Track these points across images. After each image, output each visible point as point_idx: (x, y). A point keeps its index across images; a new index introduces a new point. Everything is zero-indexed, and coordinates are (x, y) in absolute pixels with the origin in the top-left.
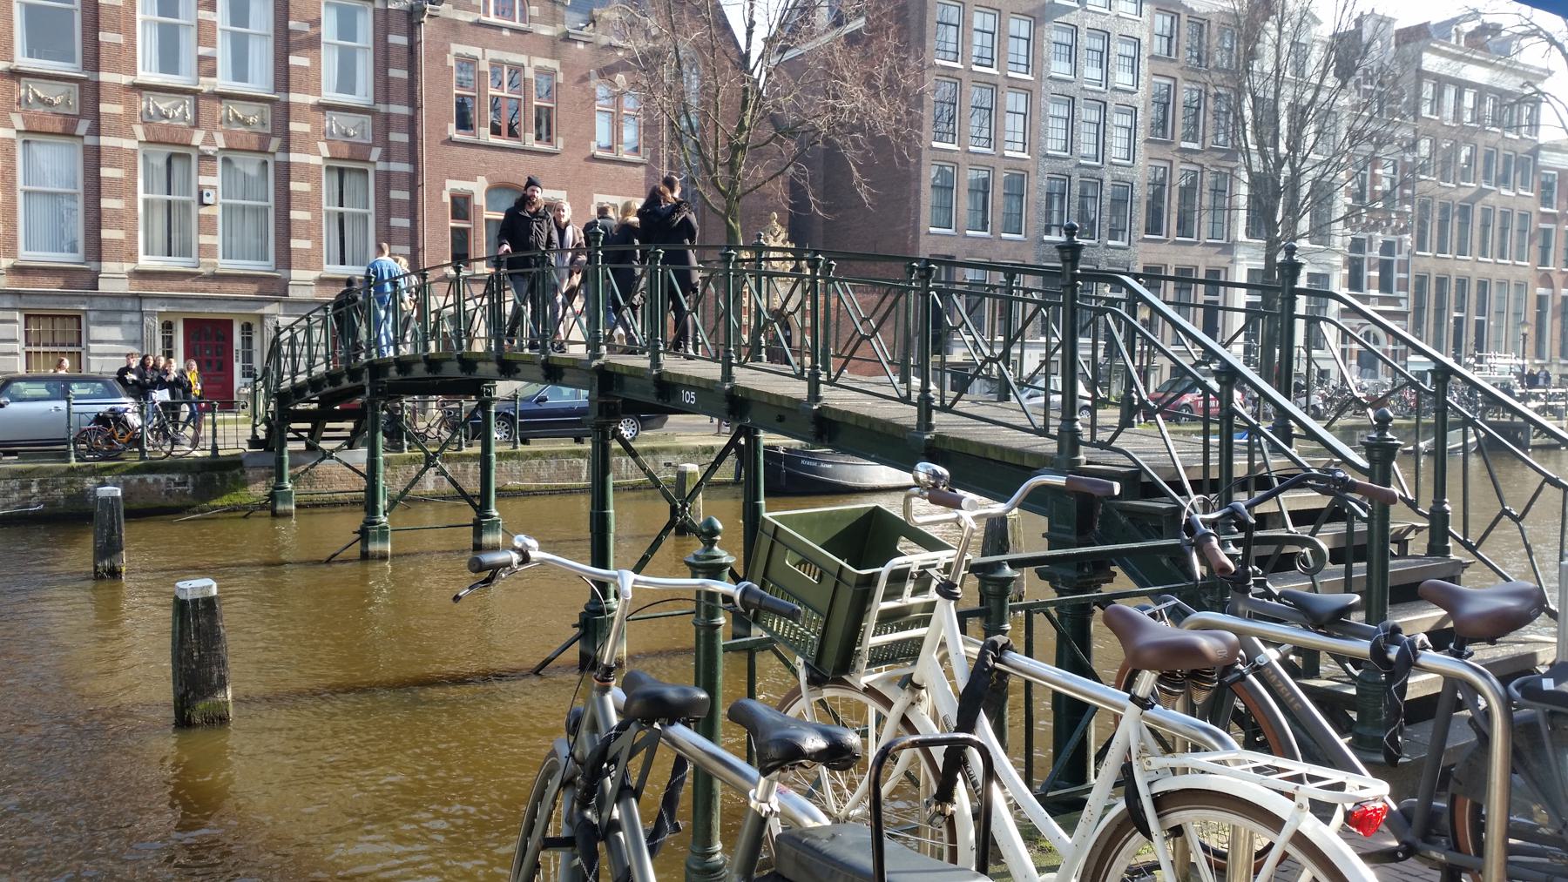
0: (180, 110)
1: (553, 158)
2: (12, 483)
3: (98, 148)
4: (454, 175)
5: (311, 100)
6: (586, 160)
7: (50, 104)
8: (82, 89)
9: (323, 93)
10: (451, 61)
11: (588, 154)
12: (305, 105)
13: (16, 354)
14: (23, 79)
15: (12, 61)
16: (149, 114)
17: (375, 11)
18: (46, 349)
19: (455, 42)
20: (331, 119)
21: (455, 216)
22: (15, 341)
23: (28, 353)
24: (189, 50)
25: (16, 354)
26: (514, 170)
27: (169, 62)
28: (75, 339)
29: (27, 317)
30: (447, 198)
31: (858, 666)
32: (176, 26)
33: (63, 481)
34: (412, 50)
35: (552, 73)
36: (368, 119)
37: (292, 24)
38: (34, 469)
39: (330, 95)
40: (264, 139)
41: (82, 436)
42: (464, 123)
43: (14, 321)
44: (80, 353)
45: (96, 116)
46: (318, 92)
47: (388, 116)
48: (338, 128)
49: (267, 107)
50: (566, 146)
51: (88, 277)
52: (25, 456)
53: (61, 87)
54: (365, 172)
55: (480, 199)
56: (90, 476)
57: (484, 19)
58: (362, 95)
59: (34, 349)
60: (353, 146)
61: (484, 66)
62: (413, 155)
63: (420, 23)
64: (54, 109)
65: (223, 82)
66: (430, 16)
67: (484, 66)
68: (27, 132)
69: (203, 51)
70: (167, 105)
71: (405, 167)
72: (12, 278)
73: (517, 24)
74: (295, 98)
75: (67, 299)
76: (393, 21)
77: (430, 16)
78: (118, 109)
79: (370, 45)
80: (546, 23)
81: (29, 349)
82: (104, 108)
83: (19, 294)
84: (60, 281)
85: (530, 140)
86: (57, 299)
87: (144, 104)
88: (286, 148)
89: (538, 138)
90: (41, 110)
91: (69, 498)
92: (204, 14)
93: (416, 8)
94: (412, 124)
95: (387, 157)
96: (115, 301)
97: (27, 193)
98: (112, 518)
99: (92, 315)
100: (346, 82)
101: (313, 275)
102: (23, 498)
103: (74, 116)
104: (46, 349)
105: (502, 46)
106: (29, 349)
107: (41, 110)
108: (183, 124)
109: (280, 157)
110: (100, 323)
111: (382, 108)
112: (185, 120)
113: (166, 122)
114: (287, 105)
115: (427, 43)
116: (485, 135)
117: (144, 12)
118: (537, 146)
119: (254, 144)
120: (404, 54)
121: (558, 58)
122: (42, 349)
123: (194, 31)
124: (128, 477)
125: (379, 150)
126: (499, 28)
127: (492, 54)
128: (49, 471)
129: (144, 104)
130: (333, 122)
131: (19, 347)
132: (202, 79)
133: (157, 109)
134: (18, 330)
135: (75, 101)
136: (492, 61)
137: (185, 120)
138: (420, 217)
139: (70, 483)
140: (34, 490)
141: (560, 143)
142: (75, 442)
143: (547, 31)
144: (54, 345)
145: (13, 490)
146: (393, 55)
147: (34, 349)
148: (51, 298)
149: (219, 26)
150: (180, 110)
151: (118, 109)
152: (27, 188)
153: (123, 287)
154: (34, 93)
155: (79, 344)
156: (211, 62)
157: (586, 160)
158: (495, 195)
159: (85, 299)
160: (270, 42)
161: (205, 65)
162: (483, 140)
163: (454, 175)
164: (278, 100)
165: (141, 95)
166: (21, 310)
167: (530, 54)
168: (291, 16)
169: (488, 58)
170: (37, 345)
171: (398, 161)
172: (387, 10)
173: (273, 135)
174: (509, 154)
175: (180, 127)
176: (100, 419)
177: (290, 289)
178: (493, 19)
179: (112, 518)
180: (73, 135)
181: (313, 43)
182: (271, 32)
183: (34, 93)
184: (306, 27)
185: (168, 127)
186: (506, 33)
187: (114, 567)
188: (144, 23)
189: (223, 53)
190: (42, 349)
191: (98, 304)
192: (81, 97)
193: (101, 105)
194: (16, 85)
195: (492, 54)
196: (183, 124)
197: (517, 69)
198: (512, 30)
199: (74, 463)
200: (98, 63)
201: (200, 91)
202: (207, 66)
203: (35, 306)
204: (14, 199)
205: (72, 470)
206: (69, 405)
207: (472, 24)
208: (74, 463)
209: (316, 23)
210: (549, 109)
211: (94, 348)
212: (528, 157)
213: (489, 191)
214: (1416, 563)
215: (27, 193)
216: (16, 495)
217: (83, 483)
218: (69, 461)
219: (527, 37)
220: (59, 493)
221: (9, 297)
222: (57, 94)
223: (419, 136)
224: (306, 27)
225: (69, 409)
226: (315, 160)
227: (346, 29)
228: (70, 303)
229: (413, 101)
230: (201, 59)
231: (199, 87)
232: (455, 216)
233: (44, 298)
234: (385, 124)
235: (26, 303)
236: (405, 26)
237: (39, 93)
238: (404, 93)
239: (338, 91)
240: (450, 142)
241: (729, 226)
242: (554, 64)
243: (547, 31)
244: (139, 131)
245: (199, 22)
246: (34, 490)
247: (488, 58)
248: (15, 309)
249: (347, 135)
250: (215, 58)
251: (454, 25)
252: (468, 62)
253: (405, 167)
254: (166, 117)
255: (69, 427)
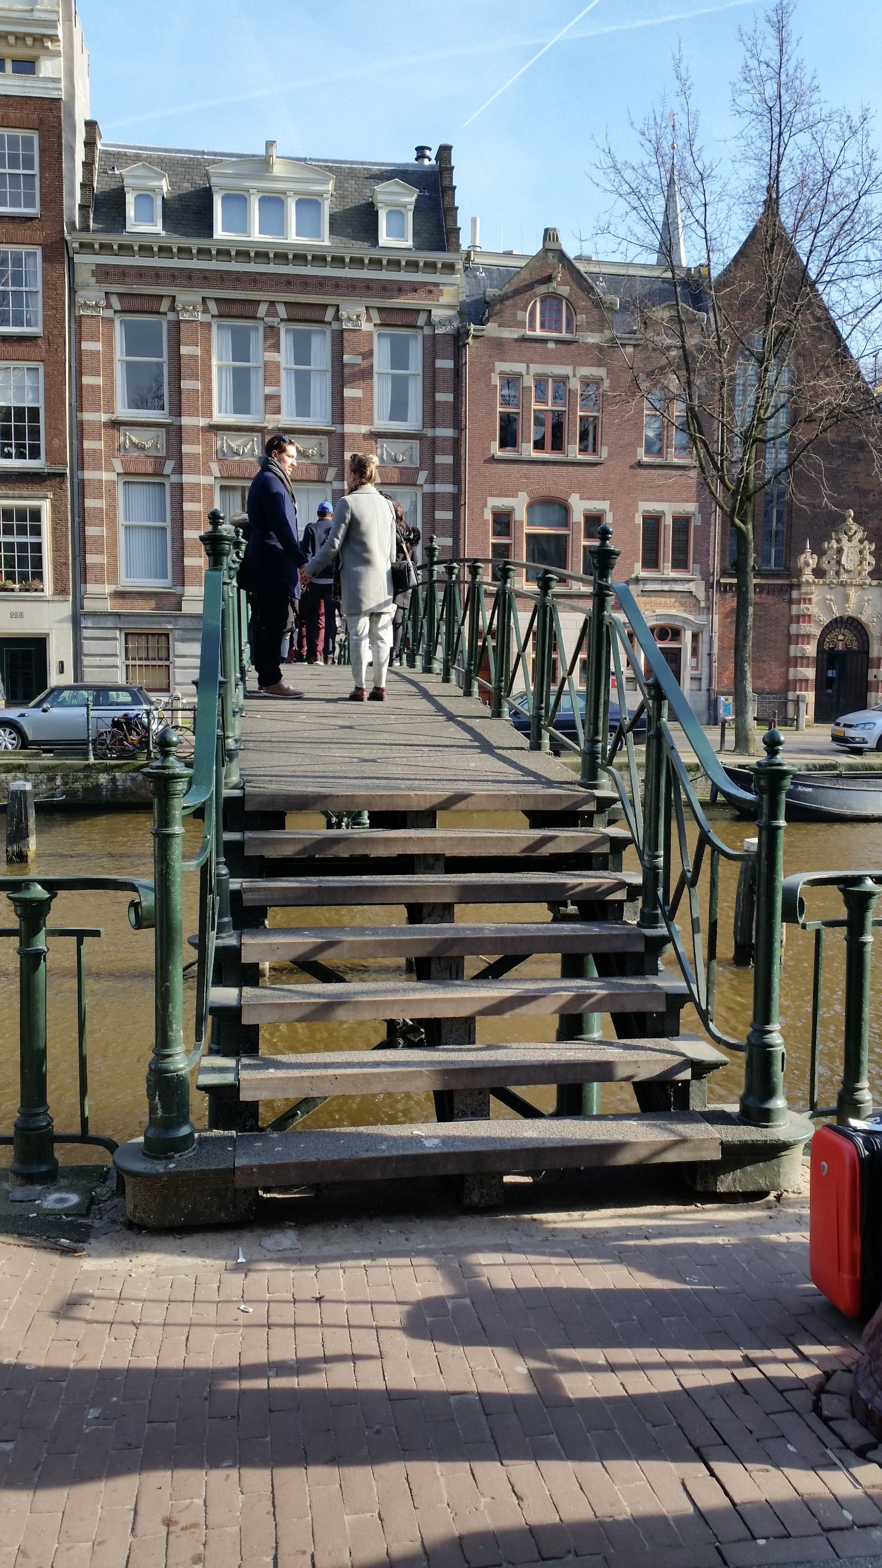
0: (249, 447)
1: (597, 468)
2: (41, 776)
3: (180, 486)
4: (496, 492)
5: (364, 429)
6: (632, 467)
7: (143, 448)
8: (168, 433)
9: (376, 421)
10: (496, 380)
11: (634, 462)
12: (358, 434)
13: (117, 667)
14: (122, 428)
15: (113, 413)
16: (223, 451)
17: (424, 337)
18: (141, 663)
19: (501, 360)
20: (382, 447)
21: (496, 533)
22: (116, 655)
23: (127, 666)
24: (259, 390)
25: (117, 667)
26: (556, 483)
27: (241, 404)
28: (163, 654)
29: (127, 635)
30: (488, 516)
31: (593, 1029)
32: (248, 369)
33: (81, 775)
34: (458, 373)
35: (598, 382)
36: (416, 444)
37: (347, 358)
38: (58, 765)
39: (382, 423)
40: (160, 462)
41: (98, 741)
42: (508, 438)
43: (115, 639)
44: (168, 666)
45: (179, 457)
46: (370, 421)
47: (434, 439)
48: (388, 454)
49: (324, 439)
50: (610, 455)
51: (173, 600)
52: (59, 754)
53: (152, 433)
54: (163, 484)
55: (521, 515)
56: (103, 772)
57: (529, 333)
58: (413, 422)
59: (131, 662)
60: (403, 471)
61: (529, 381)
62: (457, 479)
63: (465, 345)
64: (146, 452)
65: (287, 418)
66: (475, 337)
67: (529, 381)
68: (126, 474)
69: (269, 390)
70: (239, 442)
71: (449, 488)
72: (114, 601)
73: (564, 335)
74: (349, 428)
75: (156, 619)
76: (439, 346)
77: (475, 337)
78: (198, 449)
79: (420, 372)
80: (593, 331)
81: (127, 662)
82: (186, 449)
83: (118, 615)
84: (153, 603)
85: (573, 451)
86: (149, 619)
87: (219, 443)
88: (179, 470)
89: (583, 450)
90: (136, 454)
91: (86, 790)
92: (270, 356)
93: (462, 331)
94: (456, 445)
95: (432, 480)
96: (195, 620)
97: (127, 528)
98: (20, 809)
99: (176, 632)
100: (398, 411)
101: (108, 589)
102: (50, 790)
103: (414, 468)
104: (141, 663)
105: (547, 359)
106: (127, 662)
107: (136, 454)
108: (251, 459)
109: (174, 479)
110: (183, 640)
111: (429, 432)
112: (253, 455)
113: (237, 458)
114: (342, 435)
115: (471, 364)
116: (528, 450)
117: (220, 358)
118: (580, 457)
119: (314, 475)
120: (450, 377)
121: (605, 365)
122: (138, 663)
123: (261, 371)
124: (134, 774)
125: (173, 462)
126: (544, 341)
127: (536, 368)
128: (70, 767)
129: (219, 443)
130: (387, 447)
131: (120, 661)
132: (268, 416)
133: (229, 446)
134: (119, 646)
135: (162, 444)
136: (536, 375)
137: (253, 455)
138: (462, 536)
139: (86, 777)
140: (59, 782)
141: (604, 452)
142: (94, 742)
143: (593, 338)
144: (147, 659)
145: (42, 782)
146: (439, 377)
147: (131, 662)
148: (144, 619)
149: (283, 365)
150: (249, 447)
151: (198, 449)
152: (128, 523)
153: (108, 606)
154: (227, 443)
155: (168, 659)
156: (275, 401)
157: (632, 467)
158: (538, 510)
159: (171, 619)
160: (329, 375)
161: (272, 403)
162: (524, 456)
163: (496, 492)
164: (334, 432)
165: (216, 435)
166: (120, 629)
167: (575, 364)
168: (346, 350)
169: (532, 373)
170: (134, 659)
171: (443, 483)
172: (435, 335)
173: (330, 465)
174: (551, 467)
175: (250, 462)
176: (116, 724)
177: (183, 603)
178: (539, 333)
179: (20, 809)
180: (324, 482)
181: (365, 374)
182: (329, 368)
183: (130, 439)
184: (358, 360)
185: (239, 463)
186: (551, 345)
187: (21, 852)
188: (220, 368)
189: (286, 390)
190: (138, 663)
191: (181, 623)
192: (167, 440)
193: (183, 446)
194: (116, 434)
195: (536, 368)
196: (251, 459)
197: (562, 381)
198: (558, 341)
199: (92, 760)
200: (343, 417)
201: (265, 428)
202: (272, 403)
203: (132, 626)
204: (115, 533)
205: (88, 766)
206: (88, 711)
207: (517, 340)
208: (92, 760)
209: (368, 355)
210: (595, 418)
211: (179, 662)
212: (571, 469)
213: (530, 507)
214: (279, 997)
215: (127, 528)
216: (44, 787)
217: (97, 778)
218: (87, 759)
219: (573, 347)
220: (77, 785)
221: (111, 618)
222: (147, 438)
223: (463, 457)
224: (358, 360)
225: (88, 714)
226: (204, 480)
227: (399, 359)
228: (159, 623)
229: (458, 424)
230: (268, 398)
231: (265, 424)
232: (496, 533)
233: (138, 619)
234: (431, 446)
235: (124, 623)
236: (451, 349)
237: (134, 439)
238: (450, 415)
239: (392, 418)
240: (493, 460)
241: (739, 529)
242: (601, 372)
243: (593, 338)
244: (215, 467)
245: (266, 363)
246: (59, 782)
247: (532, 373)
248: (115, 628)
249: (396, 461)
250: (279, 396)
251: (499, 344)
252: (511, 380)
253: (449, 488)
254: (237, 454)
255: (88, 730)
